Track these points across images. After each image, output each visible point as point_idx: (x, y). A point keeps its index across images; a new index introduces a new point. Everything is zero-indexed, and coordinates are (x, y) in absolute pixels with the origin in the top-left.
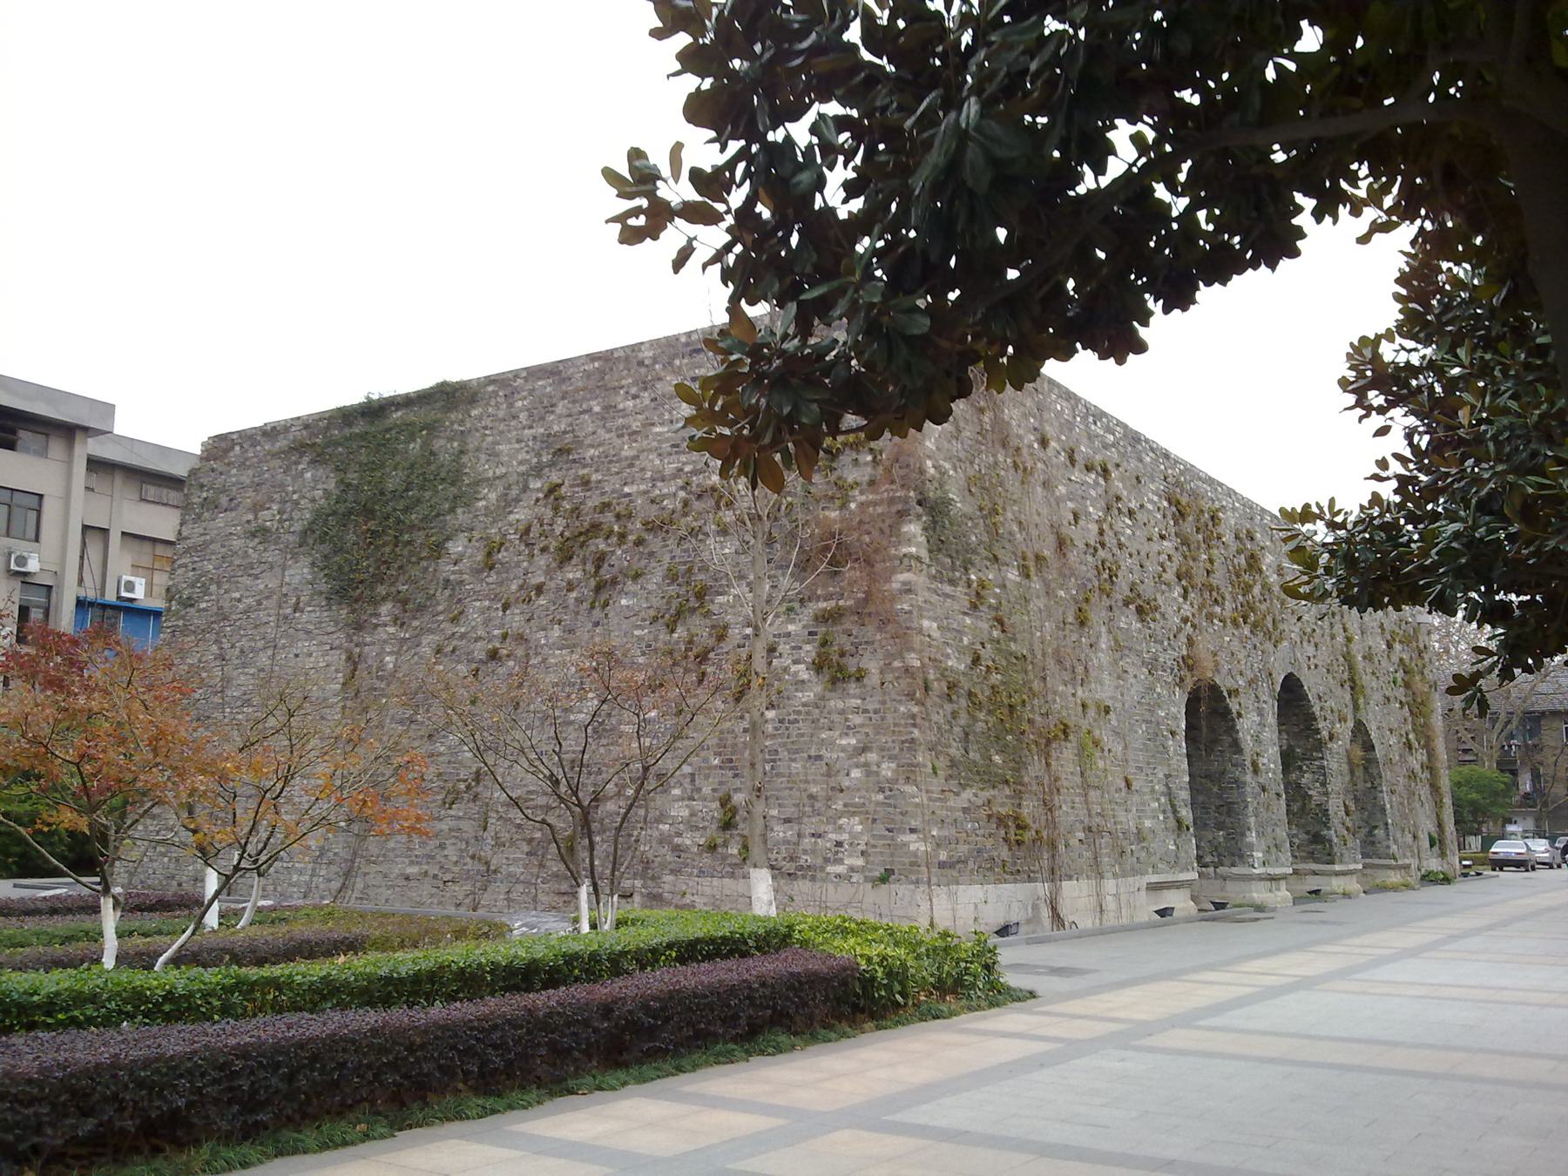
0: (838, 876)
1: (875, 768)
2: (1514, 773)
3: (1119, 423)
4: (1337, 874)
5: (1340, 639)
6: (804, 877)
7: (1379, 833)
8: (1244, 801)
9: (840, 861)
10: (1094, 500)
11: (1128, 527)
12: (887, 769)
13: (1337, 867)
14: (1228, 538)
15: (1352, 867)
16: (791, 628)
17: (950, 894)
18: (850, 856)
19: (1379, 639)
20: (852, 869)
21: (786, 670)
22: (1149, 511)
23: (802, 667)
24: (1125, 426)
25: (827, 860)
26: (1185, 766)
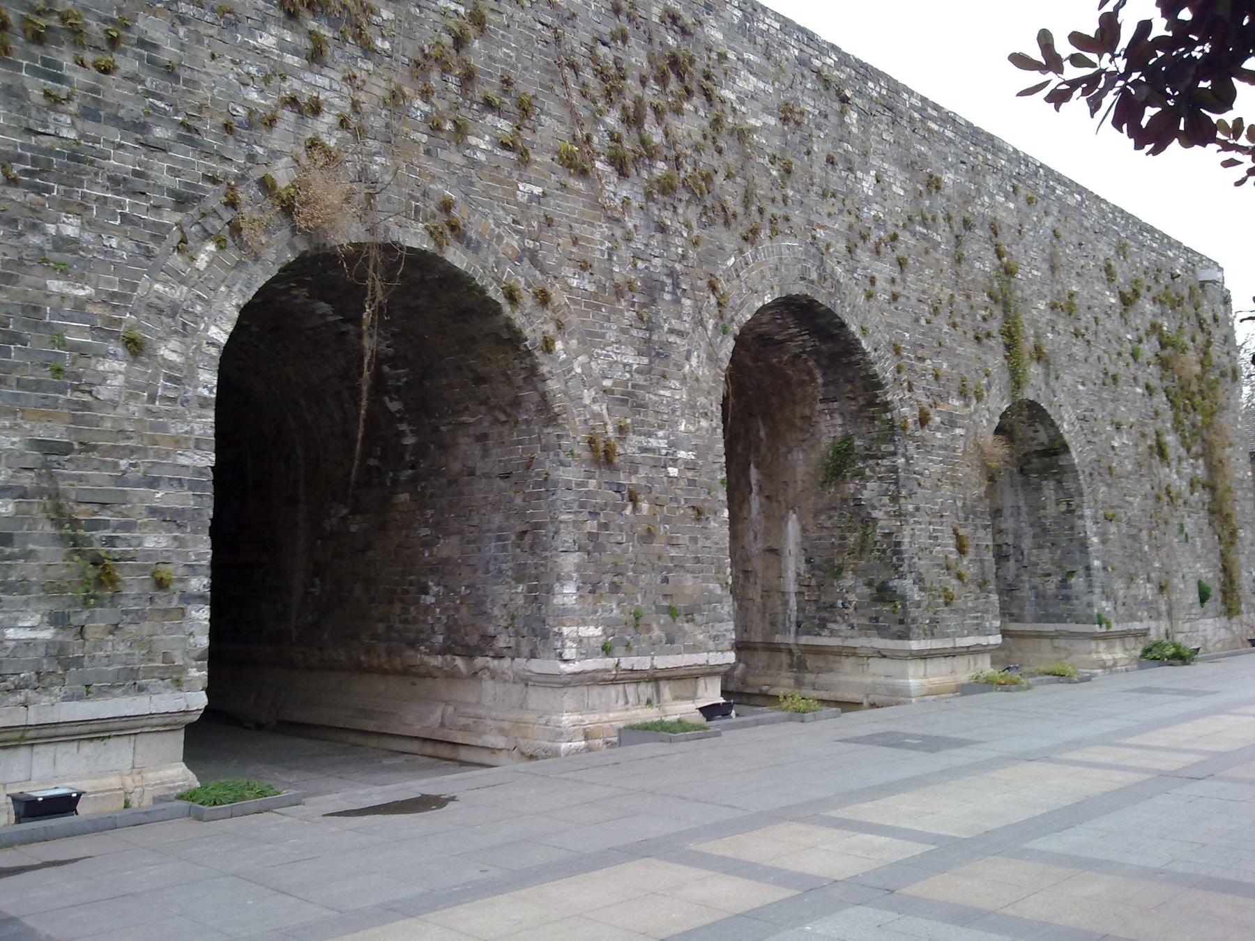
4: (924, 656)
5: (986, 265)
7: (1078, 582)
8: (554, 520)
13: (915, 645)
15: (983, 640)
26: (723, 496)
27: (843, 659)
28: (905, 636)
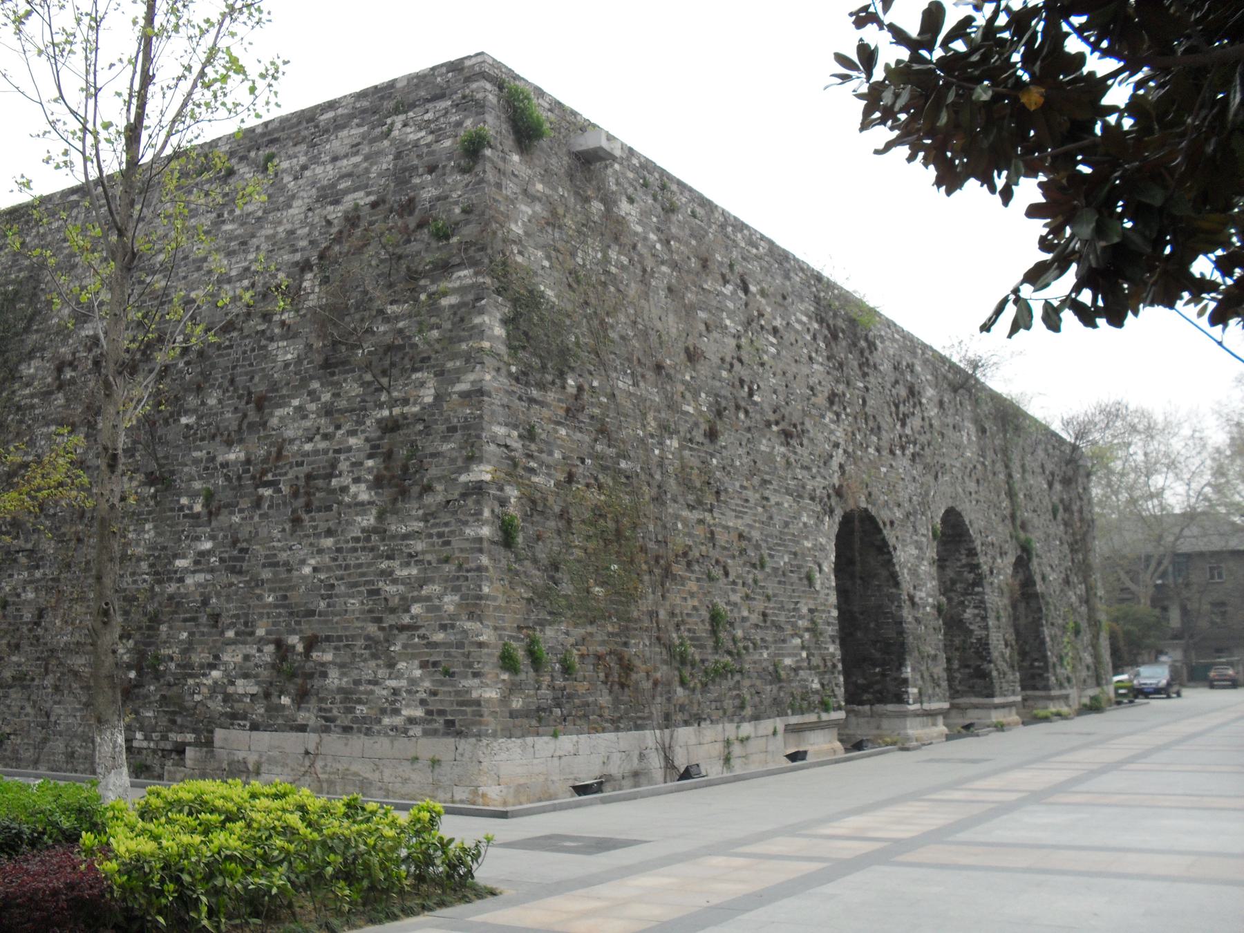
0: (394, 728)
1: (436, 602)
2: (1165, 609)
3: (763, 238)
4: (996, 707)
6: (359, 731)
9: (396, 712)
10: (731, 315)
11: (772, 345)
12: (450, 602)
13: (997, 700)
14: (886, 367)
15: (1011, 699)
16: (352, 441)
17: (524, 748)
18: (408, 706)
19: (1040, 479)
20: (411, 721)
21: (344, 489)
22: (797, 332)
23: (363, 486)
24: (771, 243)
25: (383, 711)
27: (807, 733)
28: (992, 696)
